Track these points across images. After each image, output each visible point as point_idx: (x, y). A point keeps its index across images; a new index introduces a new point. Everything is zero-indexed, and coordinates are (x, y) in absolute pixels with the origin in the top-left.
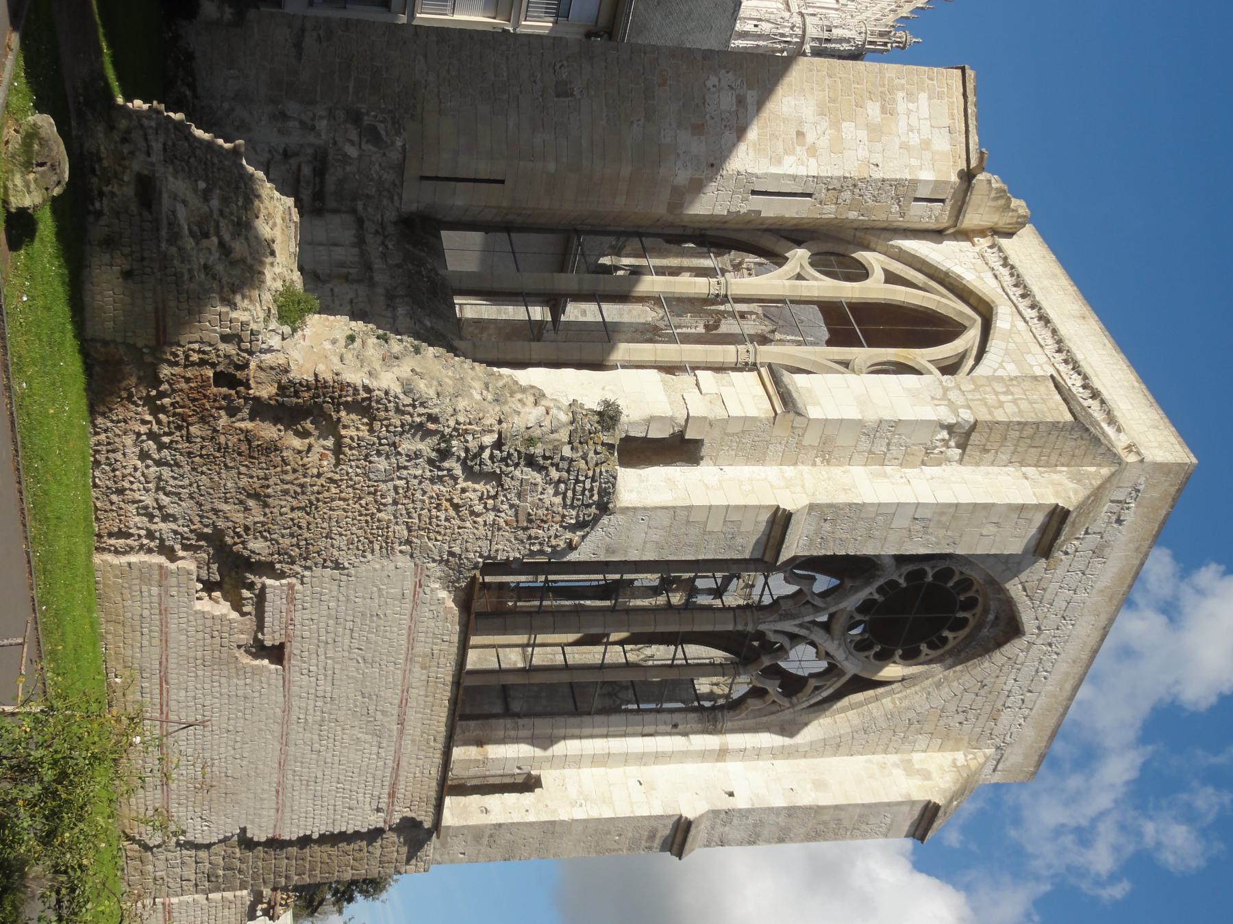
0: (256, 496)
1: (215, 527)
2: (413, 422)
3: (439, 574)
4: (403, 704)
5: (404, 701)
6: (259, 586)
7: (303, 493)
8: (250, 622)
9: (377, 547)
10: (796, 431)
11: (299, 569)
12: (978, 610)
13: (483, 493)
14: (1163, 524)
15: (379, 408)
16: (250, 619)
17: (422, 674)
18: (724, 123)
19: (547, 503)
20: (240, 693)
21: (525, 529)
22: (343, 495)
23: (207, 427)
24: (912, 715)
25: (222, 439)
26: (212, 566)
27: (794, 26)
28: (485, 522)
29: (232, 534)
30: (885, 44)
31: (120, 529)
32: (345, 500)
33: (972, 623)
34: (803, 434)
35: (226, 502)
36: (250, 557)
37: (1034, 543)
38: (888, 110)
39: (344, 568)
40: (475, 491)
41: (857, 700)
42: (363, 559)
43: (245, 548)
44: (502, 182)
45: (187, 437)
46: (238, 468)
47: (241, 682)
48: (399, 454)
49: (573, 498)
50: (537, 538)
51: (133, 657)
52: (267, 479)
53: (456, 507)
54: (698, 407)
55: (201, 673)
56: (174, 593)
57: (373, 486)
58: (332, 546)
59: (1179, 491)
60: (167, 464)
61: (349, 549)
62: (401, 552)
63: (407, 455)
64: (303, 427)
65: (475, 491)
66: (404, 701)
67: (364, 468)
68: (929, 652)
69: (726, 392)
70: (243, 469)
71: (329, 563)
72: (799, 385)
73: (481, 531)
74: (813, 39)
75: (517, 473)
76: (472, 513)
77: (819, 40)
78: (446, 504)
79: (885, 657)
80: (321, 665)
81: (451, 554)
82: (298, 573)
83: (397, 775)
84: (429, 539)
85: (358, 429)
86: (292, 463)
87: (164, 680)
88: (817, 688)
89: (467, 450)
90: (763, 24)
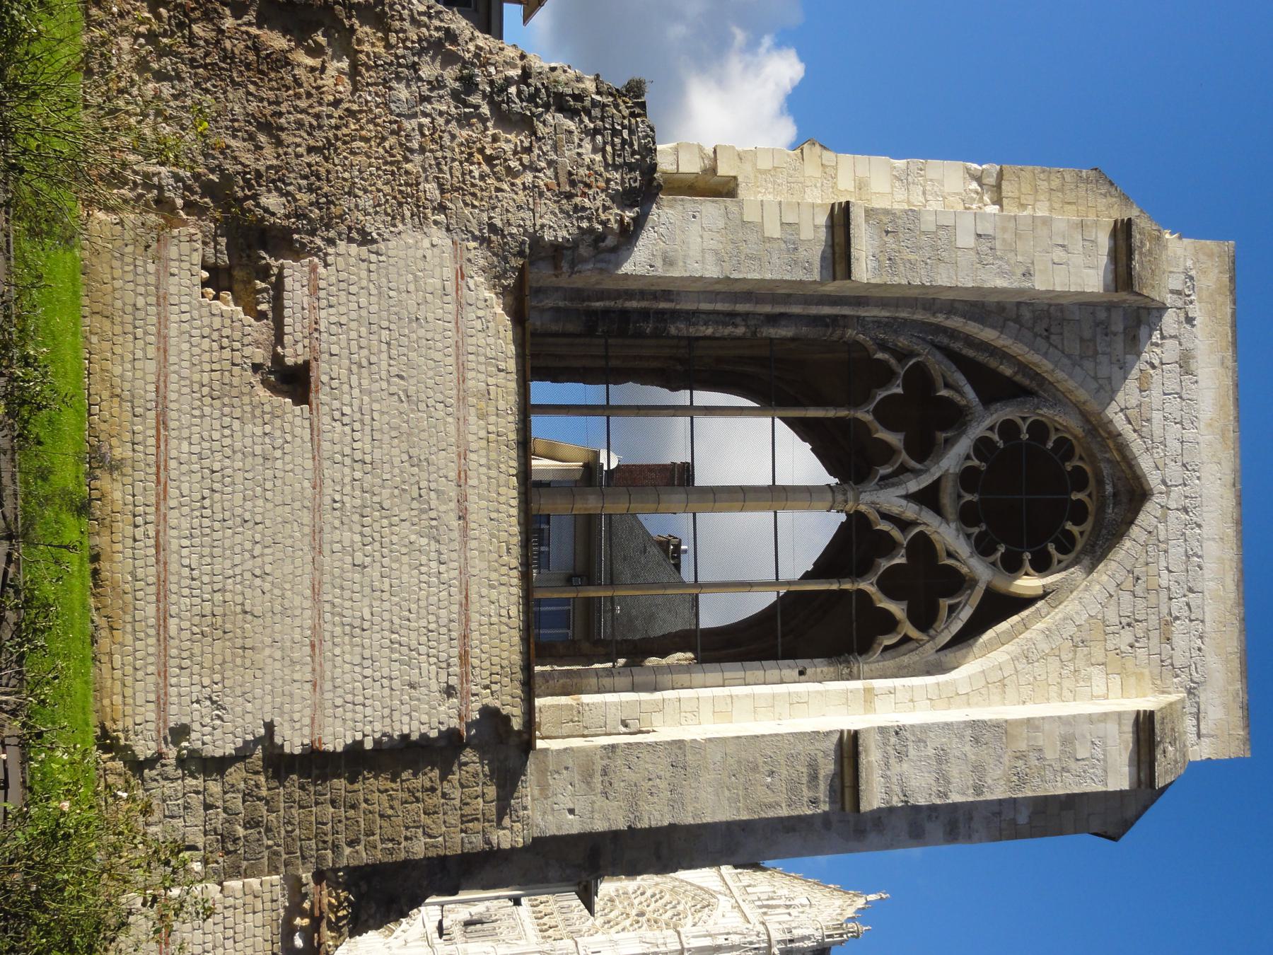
0: (266, 127)
1: (222, 171)
2: (431, 36)
3: (482, 262)
4: (462, 479)
5: (463, 475)
6: (275, 271)
7: (320, 127)
8: (263, 330)
9: (408, 214)
10: (827, 170)
11: (318, 241)
13: (516, 145)
14: (1234, 326)
15: (393, 16)
16: (267, 325)
17: (479, 427)
19: (587, 161)
20: (258, 450)
21: (569, 196)
22: (364, 133)
23: (210, 26)
24: (1072, 629)
25: (228, 44)
26: (220, 239)
27: (759, 933)
28: (523, 184)
29: (241, 183)
30: (841, 935)
31: (112, 170)
32: (367, 140)
34: (836, 175)
35: (234, 137)
36: (263, 219)
37: (1111, 277)
39: (374, 241)
40: (508, 141)
41: (1004, 629)
42: (392, 229)
43: (258, 205)
45: (189, 39)
46: (246, 87)
47: (258, 430)
48: (420, 79)
49: (614, 155)
50: (584, 209)
51: (122, 377)
52: (278, 103)
53: (489, 160)
55: (207, 410)
56: (175, 271)
57: (396, 122)
58: (357, 206)
59: (1232, 279)
60: (166, 78)
61: (376, 213)
62: (436, 223)
63: (429, 83)
64: (315, 42)
65: (508, 141)
66: (463, 475)
67: (383, 96)
70: (252, 88)
71: (354, 235)
73: (521, 197)
74: (779, 942)
75: (548, 117)
76: (509, 169)
77: (784, 941)
78: (478, 157)
79: (1012, 566)
80: (356, 403)
81: (493, 228)
82: (319, 249)
83: (468, 620)
84: (466, 204)
85: (373, 45)
86: (305, 85)
87: (162, 422)
89: (492, 83)
90: (732, 936)
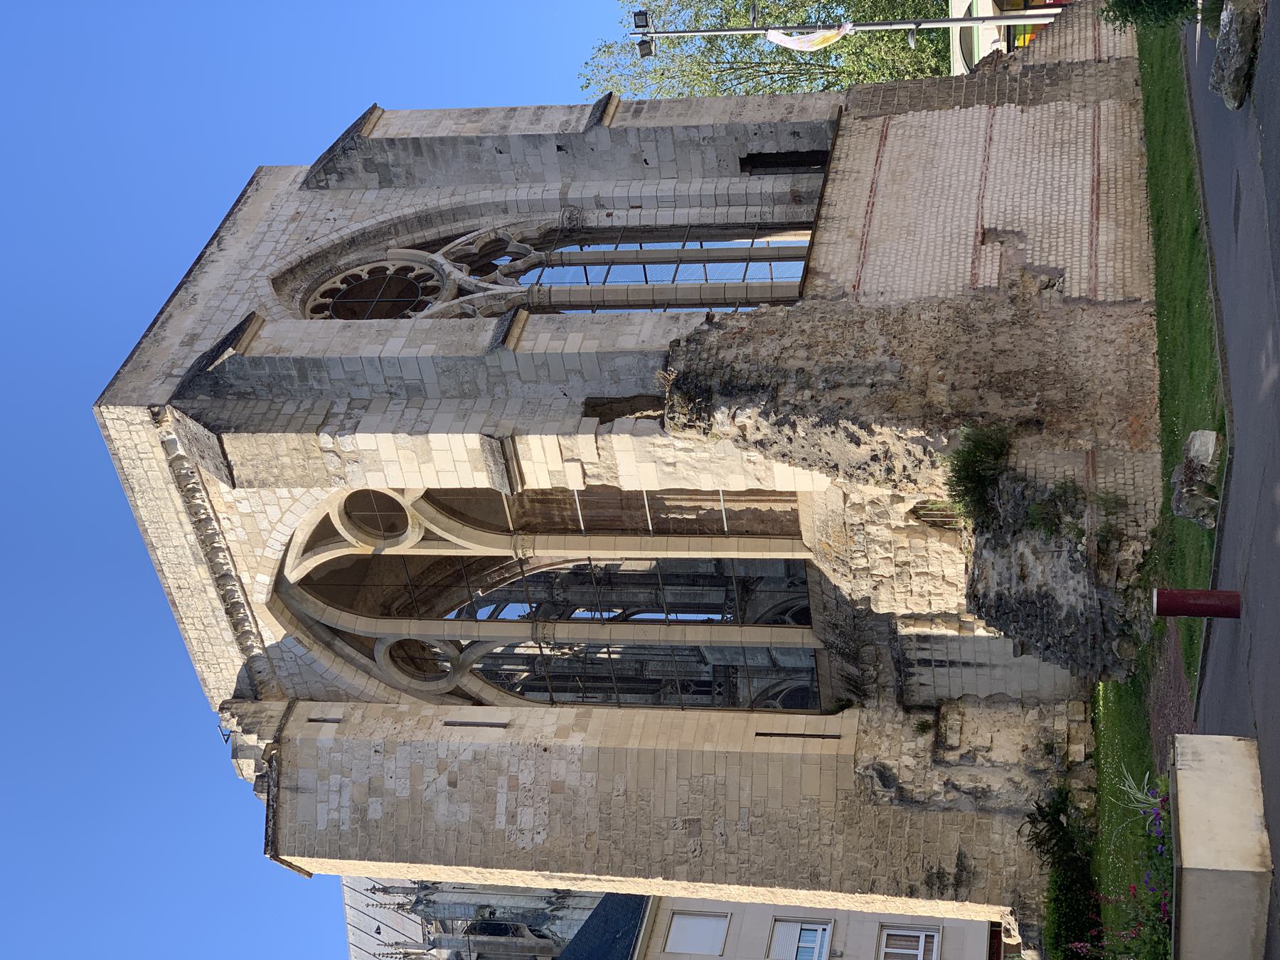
12: (310, 305)
18: (530, 794)
33: (317, 294)
38: (360, 811)
44: (757, 734)
54: (584, 444)
68: (360, 273)
69: (556, 464)
72: (485, 473)
88: (471, 244)
